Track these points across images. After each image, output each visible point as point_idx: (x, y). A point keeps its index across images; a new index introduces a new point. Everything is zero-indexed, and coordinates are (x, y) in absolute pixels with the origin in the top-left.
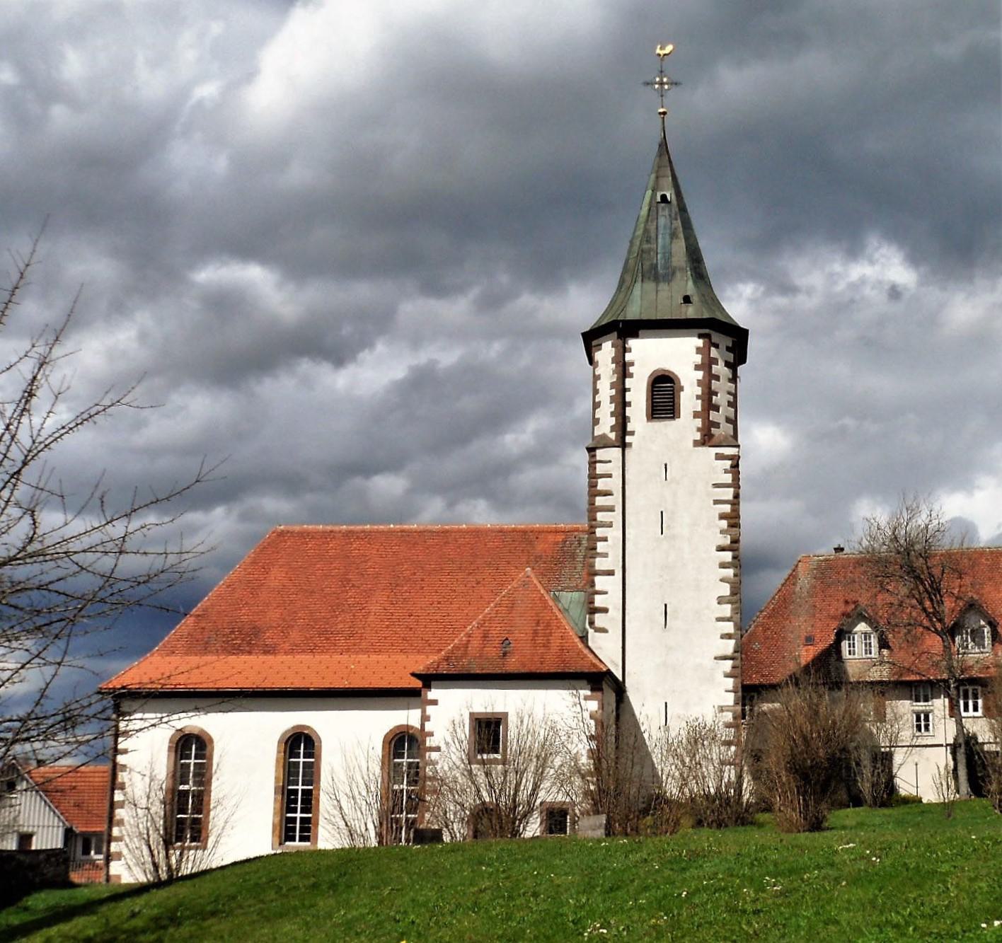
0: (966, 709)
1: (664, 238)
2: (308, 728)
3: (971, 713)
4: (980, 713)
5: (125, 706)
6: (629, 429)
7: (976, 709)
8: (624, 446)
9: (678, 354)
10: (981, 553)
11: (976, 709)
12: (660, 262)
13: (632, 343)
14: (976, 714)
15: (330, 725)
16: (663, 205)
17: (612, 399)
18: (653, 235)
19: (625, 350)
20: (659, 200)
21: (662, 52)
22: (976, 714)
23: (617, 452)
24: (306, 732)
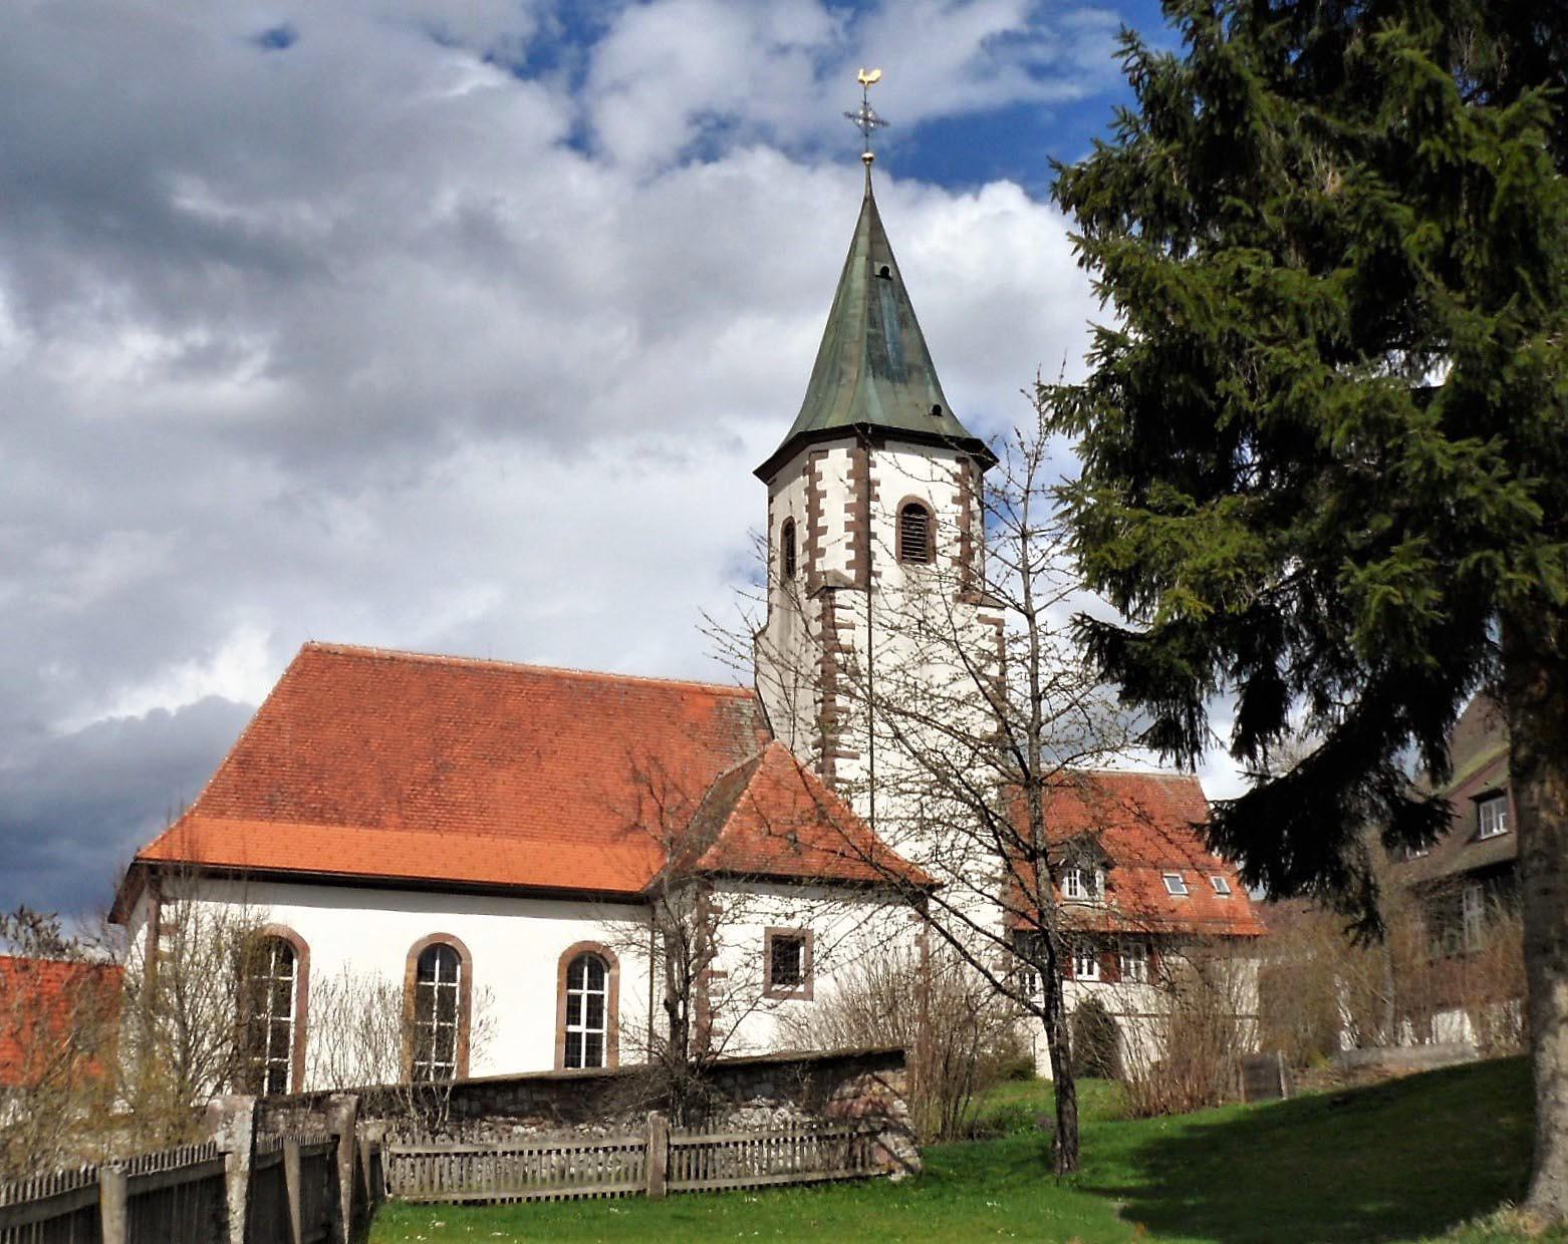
0: (1080, 972)
1: (891, 325)
2: (452, 937)
3: (1085, 976)
4: (1096, 976)
5: (717, 884)
6: (875, 568)
7: (1090, 972)
8: (869, 589)
9: (903, 475)
10: (268, 718)
11: (1090, 972)
12: (892, 355)
13: (877, 456)
14: (1091, 978)
15: (477, 931)
16: (882, 280)
17: (849, 526)
18: (878, 320)
19: (870, 464)
20: (878, 273)
21: (866, 79)
22: (1091, 978)
23: (861, 597)
24: (449, 943)
